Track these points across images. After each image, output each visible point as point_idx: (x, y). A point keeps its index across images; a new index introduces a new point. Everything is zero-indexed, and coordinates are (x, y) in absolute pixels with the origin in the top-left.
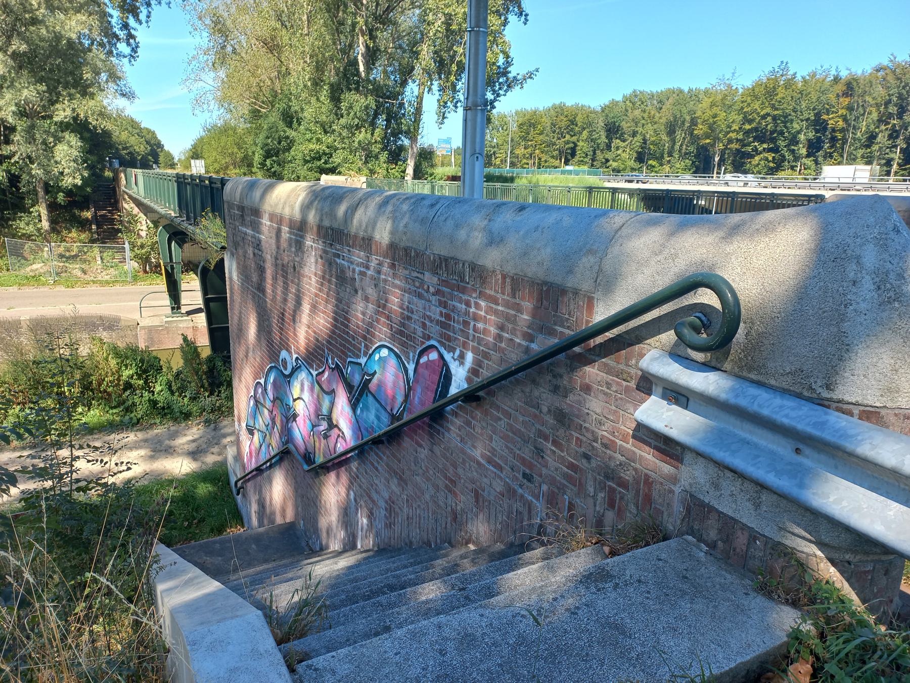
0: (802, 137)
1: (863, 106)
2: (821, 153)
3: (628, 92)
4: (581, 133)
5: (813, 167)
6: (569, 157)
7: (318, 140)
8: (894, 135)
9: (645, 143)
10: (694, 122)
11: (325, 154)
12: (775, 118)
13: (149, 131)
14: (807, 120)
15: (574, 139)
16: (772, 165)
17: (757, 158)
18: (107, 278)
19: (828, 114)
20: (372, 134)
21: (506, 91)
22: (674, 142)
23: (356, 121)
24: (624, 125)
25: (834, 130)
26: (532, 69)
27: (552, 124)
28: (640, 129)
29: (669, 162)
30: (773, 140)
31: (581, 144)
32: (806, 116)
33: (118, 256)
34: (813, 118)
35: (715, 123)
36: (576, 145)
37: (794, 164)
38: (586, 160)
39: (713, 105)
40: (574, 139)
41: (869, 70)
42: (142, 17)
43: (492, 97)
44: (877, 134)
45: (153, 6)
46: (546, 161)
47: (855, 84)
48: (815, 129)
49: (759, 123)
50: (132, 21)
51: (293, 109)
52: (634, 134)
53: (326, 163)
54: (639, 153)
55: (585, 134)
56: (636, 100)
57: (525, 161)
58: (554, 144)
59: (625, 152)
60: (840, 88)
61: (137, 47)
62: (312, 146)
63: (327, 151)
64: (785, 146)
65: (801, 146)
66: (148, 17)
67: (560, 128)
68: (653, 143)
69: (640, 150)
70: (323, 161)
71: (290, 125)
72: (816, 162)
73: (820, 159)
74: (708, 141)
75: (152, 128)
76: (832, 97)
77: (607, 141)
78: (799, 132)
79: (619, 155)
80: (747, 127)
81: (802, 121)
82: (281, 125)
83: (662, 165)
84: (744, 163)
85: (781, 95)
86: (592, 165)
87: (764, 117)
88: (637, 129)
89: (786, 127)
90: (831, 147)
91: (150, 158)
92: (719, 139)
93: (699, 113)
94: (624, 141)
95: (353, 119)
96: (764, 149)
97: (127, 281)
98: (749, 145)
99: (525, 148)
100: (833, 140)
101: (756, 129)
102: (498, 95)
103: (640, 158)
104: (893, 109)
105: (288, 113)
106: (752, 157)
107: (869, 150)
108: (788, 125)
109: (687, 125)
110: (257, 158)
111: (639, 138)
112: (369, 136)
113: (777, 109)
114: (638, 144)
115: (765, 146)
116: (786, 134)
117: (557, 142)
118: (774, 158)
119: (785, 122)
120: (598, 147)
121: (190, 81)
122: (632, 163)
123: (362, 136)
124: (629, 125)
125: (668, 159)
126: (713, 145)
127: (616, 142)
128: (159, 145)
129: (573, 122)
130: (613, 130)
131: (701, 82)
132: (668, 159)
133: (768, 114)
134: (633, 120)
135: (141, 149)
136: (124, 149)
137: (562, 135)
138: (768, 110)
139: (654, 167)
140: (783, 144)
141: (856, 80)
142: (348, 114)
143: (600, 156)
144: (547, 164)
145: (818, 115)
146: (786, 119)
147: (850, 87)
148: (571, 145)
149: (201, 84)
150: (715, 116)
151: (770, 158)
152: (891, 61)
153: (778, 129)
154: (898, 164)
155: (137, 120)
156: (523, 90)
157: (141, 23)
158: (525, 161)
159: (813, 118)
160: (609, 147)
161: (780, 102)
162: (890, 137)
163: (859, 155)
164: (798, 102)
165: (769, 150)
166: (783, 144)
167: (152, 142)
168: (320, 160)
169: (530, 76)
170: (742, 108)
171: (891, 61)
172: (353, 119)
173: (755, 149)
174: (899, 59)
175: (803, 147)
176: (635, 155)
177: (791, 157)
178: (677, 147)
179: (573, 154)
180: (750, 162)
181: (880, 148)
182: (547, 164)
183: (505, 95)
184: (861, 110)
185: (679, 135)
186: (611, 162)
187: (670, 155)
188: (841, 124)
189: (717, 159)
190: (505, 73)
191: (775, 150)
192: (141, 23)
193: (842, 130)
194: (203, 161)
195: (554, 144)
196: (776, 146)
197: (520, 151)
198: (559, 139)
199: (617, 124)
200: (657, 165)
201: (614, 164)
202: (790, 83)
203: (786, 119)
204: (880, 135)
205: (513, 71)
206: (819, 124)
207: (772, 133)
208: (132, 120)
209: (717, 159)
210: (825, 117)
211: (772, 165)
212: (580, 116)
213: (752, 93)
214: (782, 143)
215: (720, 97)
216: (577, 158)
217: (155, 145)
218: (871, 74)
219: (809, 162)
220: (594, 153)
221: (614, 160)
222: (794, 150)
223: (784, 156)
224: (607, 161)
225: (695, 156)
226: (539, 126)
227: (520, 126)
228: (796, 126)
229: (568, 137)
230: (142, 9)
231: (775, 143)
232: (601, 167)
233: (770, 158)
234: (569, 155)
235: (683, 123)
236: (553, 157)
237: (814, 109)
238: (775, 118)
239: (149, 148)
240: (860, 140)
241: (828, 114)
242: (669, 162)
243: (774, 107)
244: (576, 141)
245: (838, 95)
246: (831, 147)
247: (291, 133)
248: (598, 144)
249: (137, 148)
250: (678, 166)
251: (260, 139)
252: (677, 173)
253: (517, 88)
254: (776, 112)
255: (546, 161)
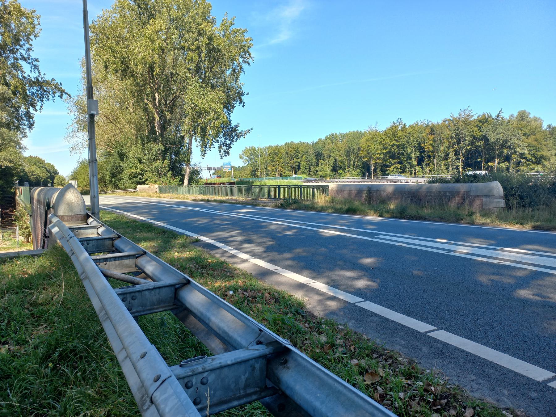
0: (413, 156)
1: (440, 139)
2: (424, 163)
3: (328, 134)
4: (302, 157)
5: (421, 170)
6: (297, 170)
7: (136, 167)
8: (457, 153)
9: (336, 161)
10: (359, 149)
11: (140, 174)
12: (398, 146)
13: (49, 165)
14: (415, 147)
15: (299, 160)
16: (400, 170)
17: (392, 167)
18: (5, 246)
19: (424, 144)
20: (163, 163)
21: (237, 139)
22: (349, 160)
23: (154, 157)
24: (324, 152)
25: (428, 152)
26: (249, 128)
27: (286, 153)
28: (332, 154)
29: (348, 171)
30: (399, 158)
31: (302, 163)
32: (413, 144)
33: (13, 235)
34: (417, 146)
35: (369, 150)
36: (300, 164)
37: (411, 170)
38: (305, 171)
39: (367, 140)
40: (299, 160)
41: (440, 122)
42: (38, 107)
43: (229, 142)
44: (449, 153)
45: (45, 102)
46: (285, 173)
47: (434, 129)
48: (419, 151)
49: (390, 149)
50: (31, 110)
51: (124, 151)
52: (330, 157)
53: (140, 179)
54: (333, 167)
55: (304, 157)
56: (332, 138)
57: (274, 173)
58: (288, 163)
59: (325, 167)
60: (428, 131)
61: (34, 123)
62: (132, 170)
63: (141, 172)
64: (405, 161)
65: (413, 160)
66: (41, 107)
67: (291, 155)
68: (340, 161)
69: (333, 165)
70: (139, 178)
71: (122, 159)
72: (422, 168)
73: (424, 167)
74: (366, 159)
75: (52, 163)
76: (424, 135)
77: (316, 161)
78: (411, 153)
79: (323, 168)
80: (385, 151)
81: (412, 147)
82: (118, 160)
83: (345, 173)
84: (386, 170)
85: (399, 135)
86: (309, 174)
87: (392, 146)
88: (331, 154)
89: (404, 151)
90: (428, 160)
91: (49, 180)
92: (372, 158)
93: (361, 145)
94: (324, 161)
95: (152, 156)
96: (395, 162)
97: (16, 247)
98: (387, 161)
99: (273, 166)
100: (429, 157)
101: (389, 152)
102: (233, 141)
103: (334, 169)
104: (454, 141)
105: (121, 154)
106: (390, 167)
107: (447, 161)
108: (405, 149)
109: (356, 151)
110: (108, 178)
111: (332, 159)
112: (161, 164)
113: (398, 142)
114: (332, 162)
115: (395, 161)
116: (405, 154)
117: (290, 162)
118: (400, 167)
119: (403, 148)
120: (311, 164)
121: (70, 137)
122: (329, 172)
123: (158, 164)
124: (326, 152)
125: (348, 169)
126: (370, 162)
127: (321, 161)
128: (56, 173)
129: (297, 151)
130: (319, 155)
131: (363, 128)
132: (348, 169)
133: (394, 145)
134: (328, 149)
135: (42, 174)
136: (33, 175)
137: (292, 158)
138: (394, 142)
139: (341, 174)
140: (404, 159)
141: (434, 126)
142: (149, 154)
143: (313, 169)
144: (285, 174)
145: (419, 144)
146: (403, 147)
147: (432, 130)
148: (298, 164)
149: (76, 139)
150: (369, 146)
151: (399, 167)
152: (451, 117)
153: (401, 152)
154: (462, 168)
155: (42, 159)
156: (245, 139)
157: (36, 111)
158: (274, 173)
159: (417, 146)
160: (317, 164)
161: (399, 138)
162: (456, 154)
163: (442, 164)
164: (408, 137)
165: (399, 163)
166: (404, 159)
167: (51, 171)
168: (137, 178)
169: (248, 132)
170: (381, 142)
171: (451, 117)
172: (152, 156)
173: (391, 163)
174: (455, 116)
175: (415, 161)
176: (331, 168)
177: (409, 166)
178: (352, 163)
179: (299, 168)
180: (389, 170)
181: (452, 160)
182: (285, 174)
183: (236, 141)
184: (439, 141)
185: (352, 157)
186: (319, 172)
187: (349, 167)
188: (431, 148)
189: (372, 169)
190: (235, 131)
191: (401, 163)
192: (36, 111)
193: (432, 152)
194: (76, 181)
195: (288, 163)
196: (401, 161)
197: (270, 168)
198: (290, 160)
199: (320, 152)
200: (343, 173)
201: (321, 173)
202: (404, 129)
203: (403, 147)
204: (450, 154)
205: (239, 130)
206: (421, 149)
207: (398, 154)
208: (39, 159)
209: (372, 169)
210: (422, 145)
211: (400, 170)
212: (300, 148)
213: (386, 134)
214: (404, 159)
215: (370, 136)
216: (300, 171)
217: (53, 172)
218: (442, 123)
219: (418, 168)
220: (310, 168)
221: (321, 171)
222: (410, 162)
223: (405, 166)
224: (317, 171)
225: (362, 167)
226: (280, 154)
227: (269, 154)
228: (409, 150)
229: (295, 159)
230: (38, 103)
231: (400, 159)
232: (314, 175)
233: (399, 167)
234: (297, 169)
235: (354, 150)
236: (288, 170)
237: (417, 141)
238: (398, 146)
239: (49, 174)
240: (441, 157)
241: (424, 144)
242: (348, 171)
243: (397, 141)
244: (299, 161)
245: (427, 134)
246: (428, 160)
247: (122, 164)
248: (311, 163)
249: (41, 175)
250: (354, 173)
251: (109, 167)
252: (354, 176)
253: (242, 138)
254: (397, 143)
255: (285, 173)
